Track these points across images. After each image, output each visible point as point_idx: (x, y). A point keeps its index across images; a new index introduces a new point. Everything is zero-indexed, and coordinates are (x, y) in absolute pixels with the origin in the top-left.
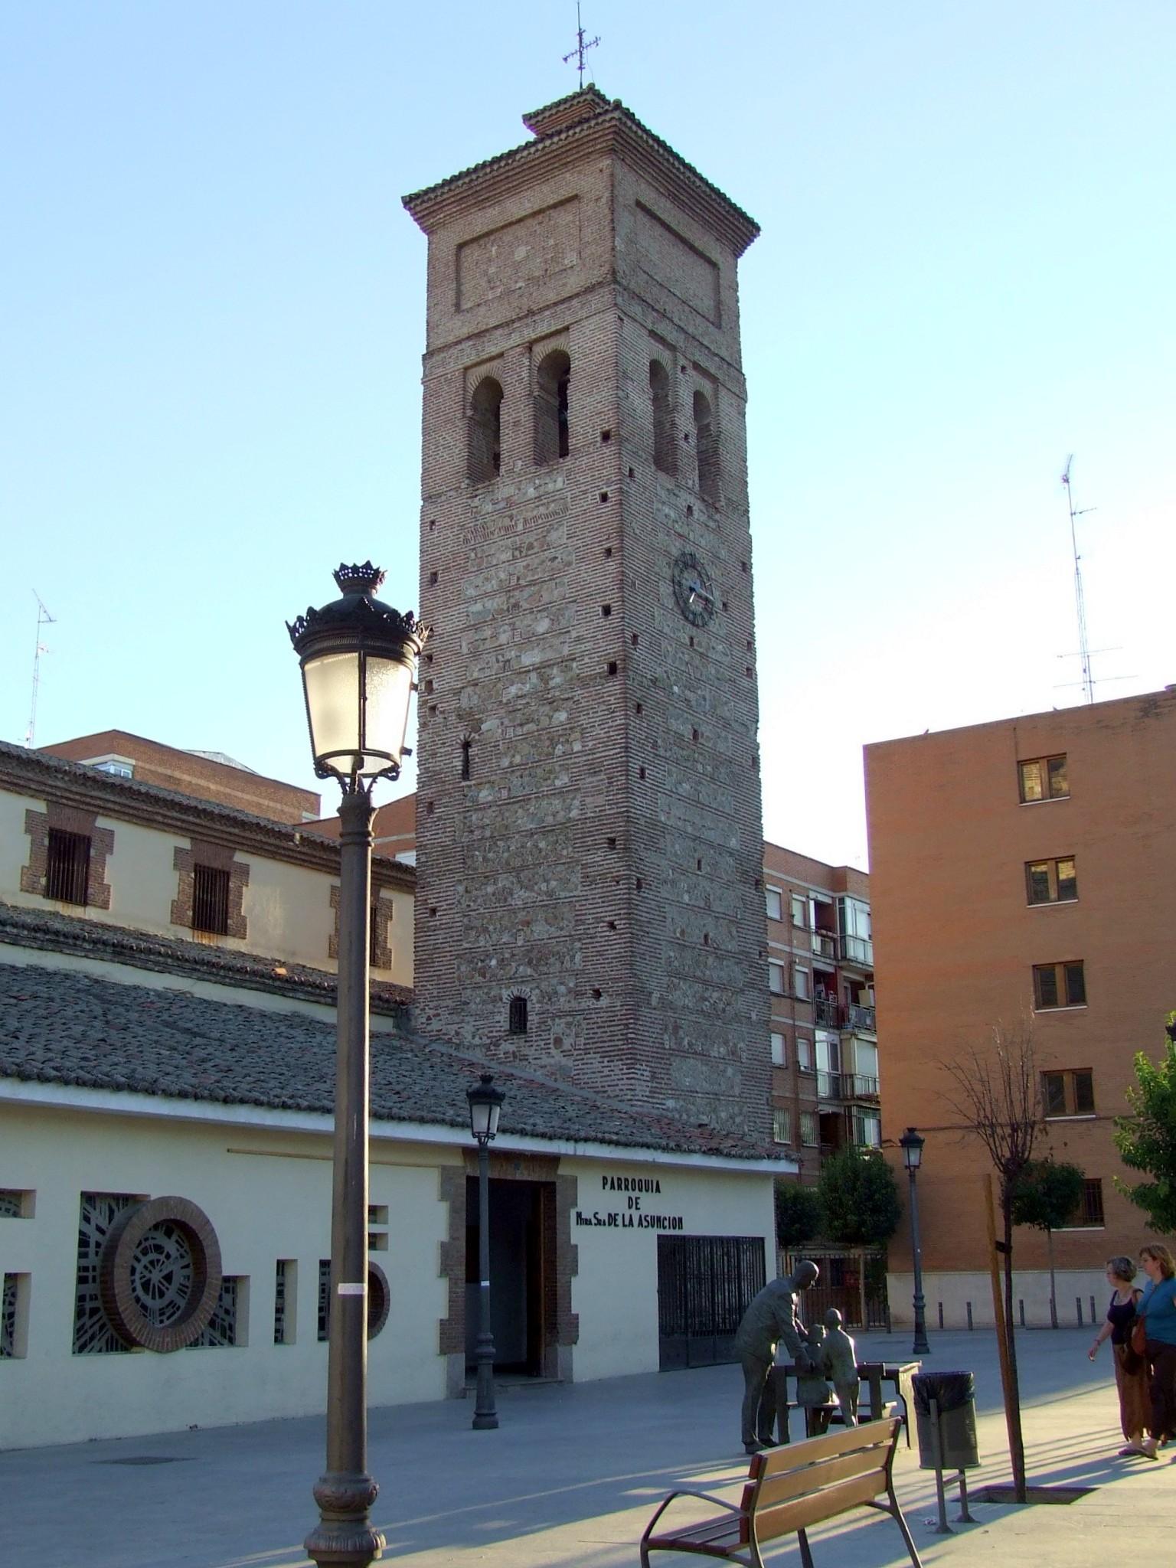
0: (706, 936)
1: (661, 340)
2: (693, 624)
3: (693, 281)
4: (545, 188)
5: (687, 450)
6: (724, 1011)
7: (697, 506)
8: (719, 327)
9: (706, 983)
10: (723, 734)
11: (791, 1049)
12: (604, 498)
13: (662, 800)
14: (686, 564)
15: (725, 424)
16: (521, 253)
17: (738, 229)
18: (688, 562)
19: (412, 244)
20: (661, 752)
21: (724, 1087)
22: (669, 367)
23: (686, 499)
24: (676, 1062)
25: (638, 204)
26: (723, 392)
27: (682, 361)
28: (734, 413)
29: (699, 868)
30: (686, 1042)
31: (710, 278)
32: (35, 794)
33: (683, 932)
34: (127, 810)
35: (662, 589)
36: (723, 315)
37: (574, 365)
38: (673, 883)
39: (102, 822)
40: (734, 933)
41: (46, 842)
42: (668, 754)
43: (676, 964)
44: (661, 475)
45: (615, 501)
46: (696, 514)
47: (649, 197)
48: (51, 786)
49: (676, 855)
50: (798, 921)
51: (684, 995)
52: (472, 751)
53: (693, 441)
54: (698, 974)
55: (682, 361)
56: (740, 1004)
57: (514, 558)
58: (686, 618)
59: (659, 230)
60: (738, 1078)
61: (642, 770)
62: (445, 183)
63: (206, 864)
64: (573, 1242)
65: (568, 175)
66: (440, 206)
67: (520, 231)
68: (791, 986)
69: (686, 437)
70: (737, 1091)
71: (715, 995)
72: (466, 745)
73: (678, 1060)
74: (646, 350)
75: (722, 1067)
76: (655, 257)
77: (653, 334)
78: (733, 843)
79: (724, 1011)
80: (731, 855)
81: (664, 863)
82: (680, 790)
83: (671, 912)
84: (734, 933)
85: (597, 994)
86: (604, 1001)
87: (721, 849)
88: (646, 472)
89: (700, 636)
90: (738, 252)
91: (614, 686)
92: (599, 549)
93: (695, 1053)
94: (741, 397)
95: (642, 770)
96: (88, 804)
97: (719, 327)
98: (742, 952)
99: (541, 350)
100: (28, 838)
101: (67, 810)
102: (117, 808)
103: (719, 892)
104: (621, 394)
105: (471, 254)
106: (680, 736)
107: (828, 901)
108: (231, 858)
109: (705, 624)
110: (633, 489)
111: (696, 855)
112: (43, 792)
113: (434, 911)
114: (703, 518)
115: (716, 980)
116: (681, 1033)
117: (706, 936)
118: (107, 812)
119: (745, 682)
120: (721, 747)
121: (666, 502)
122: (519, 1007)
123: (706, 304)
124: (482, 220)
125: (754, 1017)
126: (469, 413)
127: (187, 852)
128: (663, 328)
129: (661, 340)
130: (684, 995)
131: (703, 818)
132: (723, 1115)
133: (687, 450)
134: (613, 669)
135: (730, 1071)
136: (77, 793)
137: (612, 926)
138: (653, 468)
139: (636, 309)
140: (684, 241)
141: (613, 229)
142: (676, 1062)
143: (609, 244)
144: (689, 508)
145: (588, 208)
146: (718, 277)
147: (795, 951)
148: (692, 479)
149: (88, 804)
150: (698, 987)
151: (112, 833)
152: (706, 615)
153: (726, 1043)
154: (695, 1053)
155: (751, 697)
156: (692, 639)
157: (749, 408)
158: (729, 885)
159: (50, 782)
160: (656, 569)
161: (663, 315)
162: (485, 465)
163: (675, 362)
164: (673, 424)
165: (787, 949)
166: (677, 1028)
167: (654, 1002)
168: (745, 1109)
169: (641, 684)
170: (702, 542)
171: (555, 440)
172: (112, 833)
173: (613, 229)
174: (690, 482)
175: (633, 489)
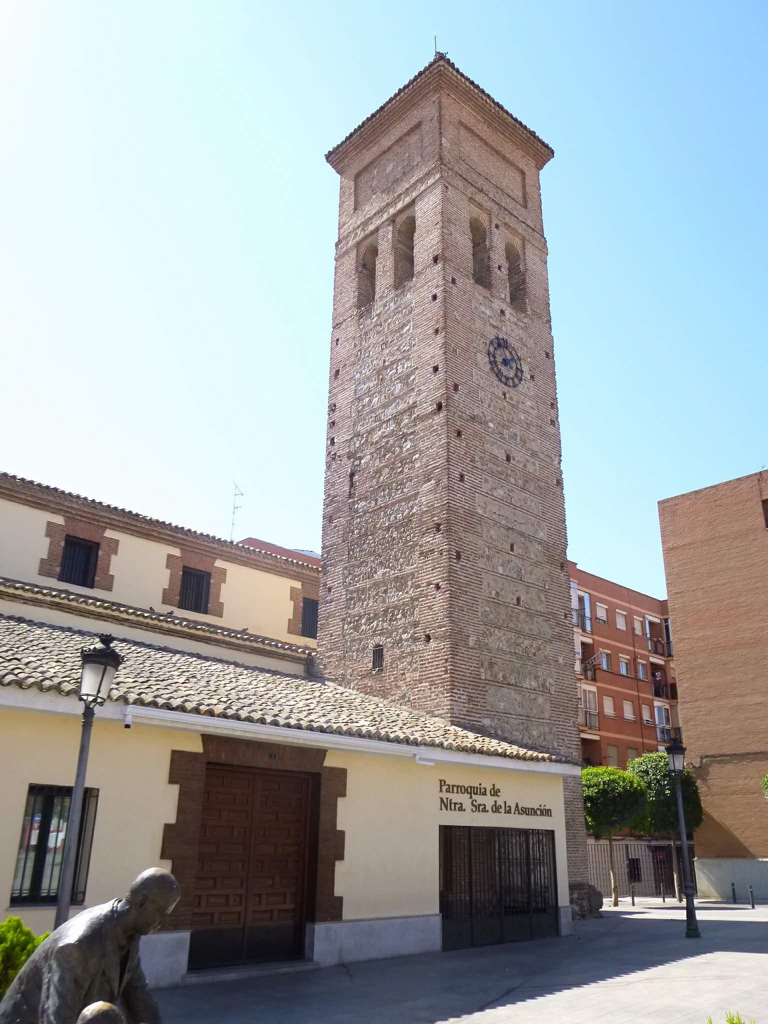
0: (518, 599)
1: (480, 206)
2: (506, 384)
3: (510, 182)
4: (403, 124)
5: (501, 275)
6: (535, 654)
7: (508, 311)
8: (526, 207)
9: (519, 632)
10: (532, 460)
11: (638, 712)
12: (435, 297)
13: (478, 498)
14: (499, 345)
15: (530, 265)
16: (389, 168)
17: (542, 153)
18: (501, 344)
19: (332, 179)
20: (479, 465)
21: (535, 711)
22: (486, 224)
23: (497, 305)
24: (491, 690)
25: (461, 123)
26: (528, 246)
27: (495, 221)
28: (537, 260)
29: (512, 550)
30: (501, 675)
31: (519, 179)
32: (55, 511)
33: (497, 593)
34: (129, 527)
35: (479, 359)
36: (530, 199)
37: (418, 222)
38: (489, 558)
39: (109, 534)
40: (543, 599)
41: (63, 544)
42: (485, 468)
43: (491, 616)
44: (480, 288)
45: (446, 300)
46: (508, 315)
47: (470, 121)
48: (68, 507)
49: (491, 538)
50: (638, 632)
51: (499, 640)
52: (356, 477)
53: (505, 271)
54: (511, 625)
55: (495, 221)
56: (548, 650)
57: (382, 349)
58: (500, 380)
59: (478, 144)
60: (548, 706)
61: (462, 476)
62: (347, 138)
63: (192, 566)
64: (339, 827)
65: (415, 112)
66: (346, 153)
67: (390, 155)
68: (636, 672)
69: (499, 268)
70: (547, 715)
71: (527, 642)
72: (352, 475)
73: (493, 688)
74: (465, 212)
75: (533, 696)
76: (476, 159)
77: (471, 199)
78: (541, 535)
79: (535, 654)
80: (540, 543)
81: (480, 542)
82: (495, 494)
83: (487, 578)
84: (543, 599)
85: (428, 638)
86: (433, 644)
87: (529, 538)
88: (466, 283)
89: (511, 393)
90: (540, 167)
91: (440, 418)
92: (431, 331)
93: (509, 684)
94: (543, 248)
95: (462, 476)
96: (98, 521)
97: (526, 207)
98: (550, 613)
99: (400, 220)
100: (48, 540)
101: (81, 524)
102: (121, 525)
103: (529, 569)
104: (445, 231)
105: (365, 178)
106: (496, 457)
107: (658, 621)
108: (213, 563)
109: (515, 386)
110: (455, 290)
111: (510, 541)
112: (61, 510)
113: (330, 589)
114: (514, 319)
115: (527, 631)
116: (496, 667)
117: (518, 599)
118: (114, 527)
119: (551, 430)
120: (530, 468)
121: (490, 311)
122: (378, 654)
123: (518, 193)
124: (368, 156)
125: (561, 661)
126: (360, 269)
127: (177, 558)
128: (479, 197)
129: (480, 206)
130: (499, 640)
131: (515, 514)
132: (535, 733)
133: (501, 275)
134: (440, 407)
135: (540, 700)
136: (88, 513)
137: (438, 587)
138: (472, 281)
139: (460, 184)
140: (498, 153)
141: (441, 133)
142: (491, 690)
143: (438, 143)
144: (502, 312)
145: (425, 127)
146: (524, 179)
147: (637, 650)
148: (505, 293)
149: (98, 521)
150: (512, 636)
151: (117, 542)
152: (516, 381)
153: (536, 678)
154: (509, 684)
155: (556, 441)
156: (504, 394)
157: (549, 259)
158: (537, 564)
159: (66, 504)
160: (474, 345)
161: (481, 191)
162: (366, 298)
163: (490, 222)
164: (489, 258)
165: (632, 649)
166: (491, 665)
167: (471, 643)
168: (555, 729)
169: (461, 417)
170: (512, 328)
171: (405, 270)
172: (117, 542)
173: (441, 133)
174: (503, 296)
175: (455, 290)
